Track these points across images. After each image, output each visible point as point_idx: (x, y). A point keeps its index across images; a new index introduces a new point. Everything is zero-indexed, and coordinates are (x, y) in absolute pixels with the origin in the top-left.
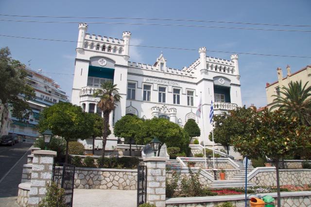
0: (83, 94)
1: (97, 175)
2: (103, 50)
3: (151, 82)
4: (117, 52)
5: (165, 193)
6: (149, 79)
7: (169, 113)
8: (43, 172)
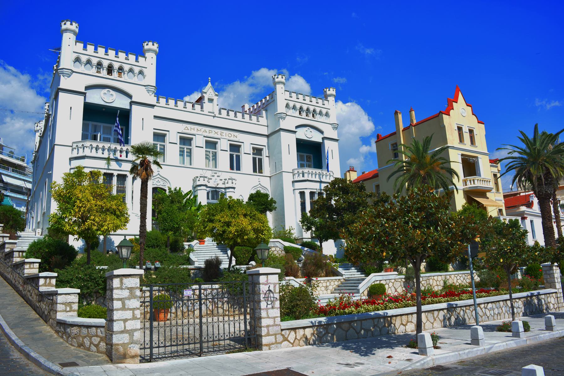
0: (75, 154)
2: (108, 74)
5: (279, 315)
6: (189, 126)
7: (223, 186)
8: (129, 299)
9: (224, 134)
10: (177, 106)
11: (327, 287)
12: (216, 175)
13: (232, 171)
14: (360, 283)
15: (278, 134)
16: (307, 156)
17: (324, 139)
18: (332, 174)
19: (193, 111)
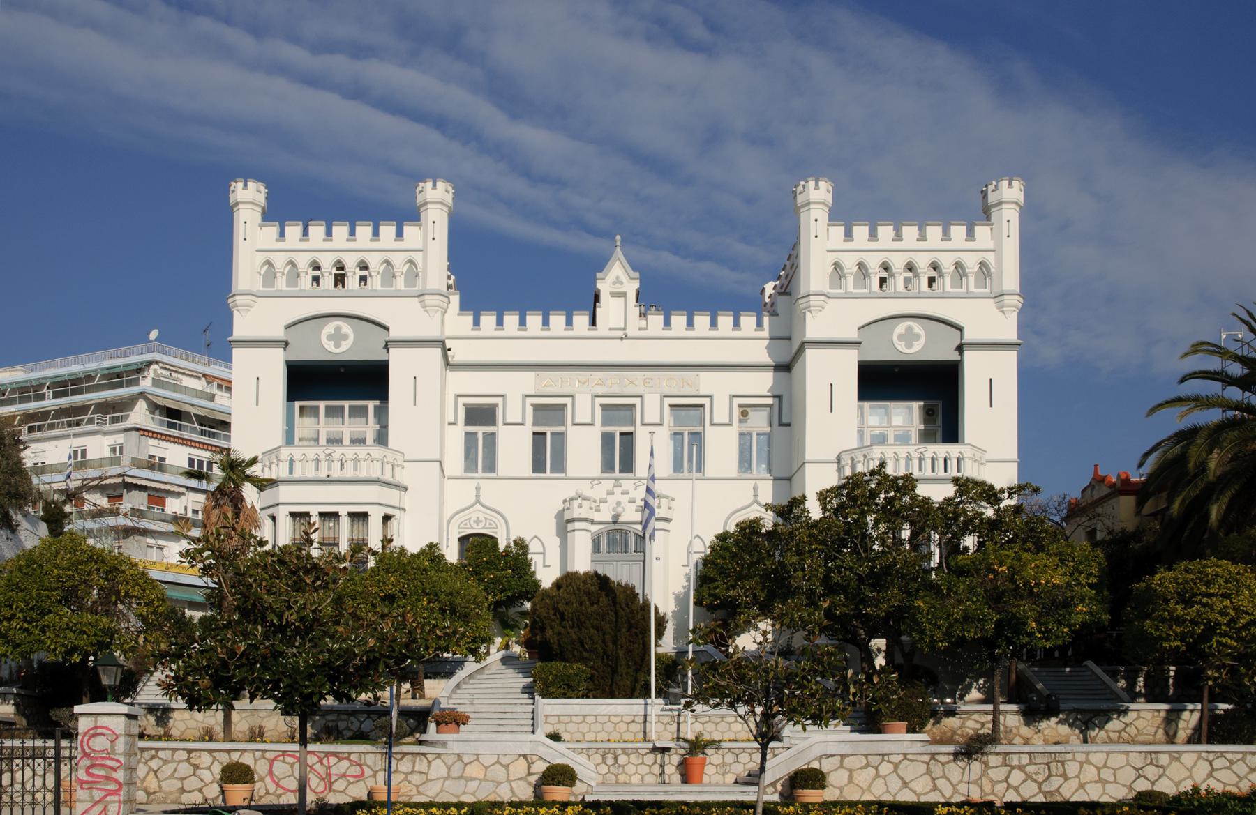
1: (173, 761)
4: (400, 283)
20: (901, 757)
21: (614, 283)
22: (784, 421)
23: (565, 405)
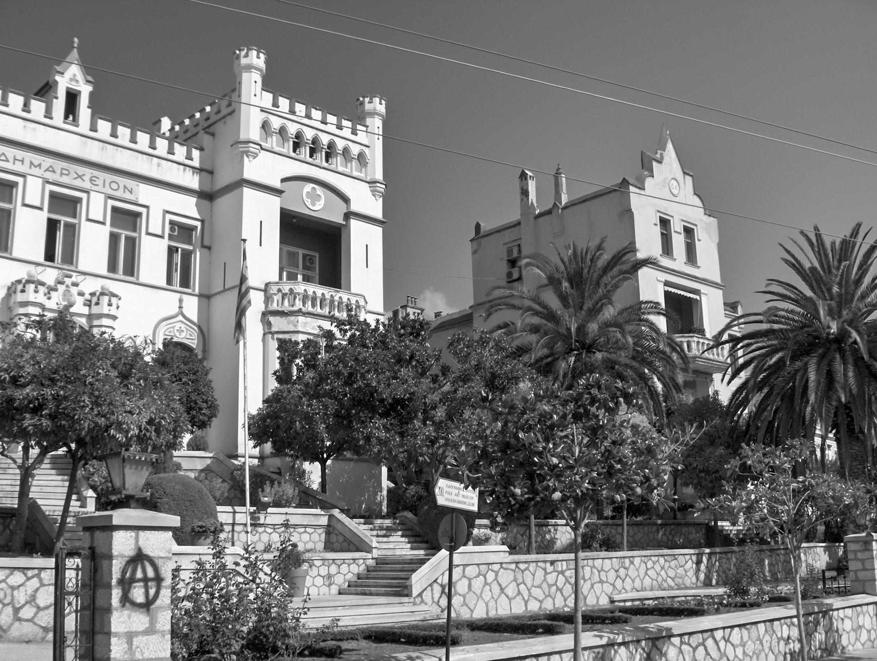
3: (18, 167)
9: (99, 182)
10: (29, 112)
11: (329, 576)
12: (68, 281)
13: (112, 275)
14: (414, 571)
15: (237, 191)
16: (304, 256)
17: (348, 215)
18: (362, 303)
19: (92, 134)
20: (499, 566)
21: (71, 80)
22: (206, 243)
23: (17, 183)
